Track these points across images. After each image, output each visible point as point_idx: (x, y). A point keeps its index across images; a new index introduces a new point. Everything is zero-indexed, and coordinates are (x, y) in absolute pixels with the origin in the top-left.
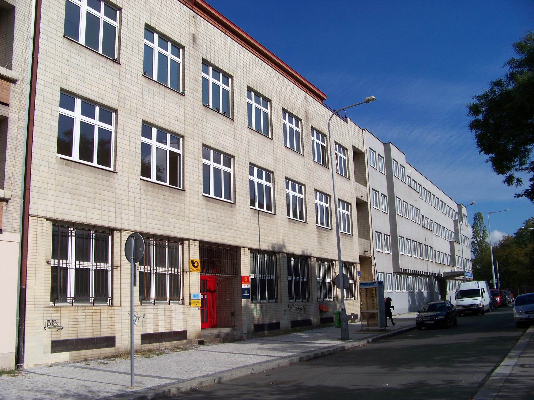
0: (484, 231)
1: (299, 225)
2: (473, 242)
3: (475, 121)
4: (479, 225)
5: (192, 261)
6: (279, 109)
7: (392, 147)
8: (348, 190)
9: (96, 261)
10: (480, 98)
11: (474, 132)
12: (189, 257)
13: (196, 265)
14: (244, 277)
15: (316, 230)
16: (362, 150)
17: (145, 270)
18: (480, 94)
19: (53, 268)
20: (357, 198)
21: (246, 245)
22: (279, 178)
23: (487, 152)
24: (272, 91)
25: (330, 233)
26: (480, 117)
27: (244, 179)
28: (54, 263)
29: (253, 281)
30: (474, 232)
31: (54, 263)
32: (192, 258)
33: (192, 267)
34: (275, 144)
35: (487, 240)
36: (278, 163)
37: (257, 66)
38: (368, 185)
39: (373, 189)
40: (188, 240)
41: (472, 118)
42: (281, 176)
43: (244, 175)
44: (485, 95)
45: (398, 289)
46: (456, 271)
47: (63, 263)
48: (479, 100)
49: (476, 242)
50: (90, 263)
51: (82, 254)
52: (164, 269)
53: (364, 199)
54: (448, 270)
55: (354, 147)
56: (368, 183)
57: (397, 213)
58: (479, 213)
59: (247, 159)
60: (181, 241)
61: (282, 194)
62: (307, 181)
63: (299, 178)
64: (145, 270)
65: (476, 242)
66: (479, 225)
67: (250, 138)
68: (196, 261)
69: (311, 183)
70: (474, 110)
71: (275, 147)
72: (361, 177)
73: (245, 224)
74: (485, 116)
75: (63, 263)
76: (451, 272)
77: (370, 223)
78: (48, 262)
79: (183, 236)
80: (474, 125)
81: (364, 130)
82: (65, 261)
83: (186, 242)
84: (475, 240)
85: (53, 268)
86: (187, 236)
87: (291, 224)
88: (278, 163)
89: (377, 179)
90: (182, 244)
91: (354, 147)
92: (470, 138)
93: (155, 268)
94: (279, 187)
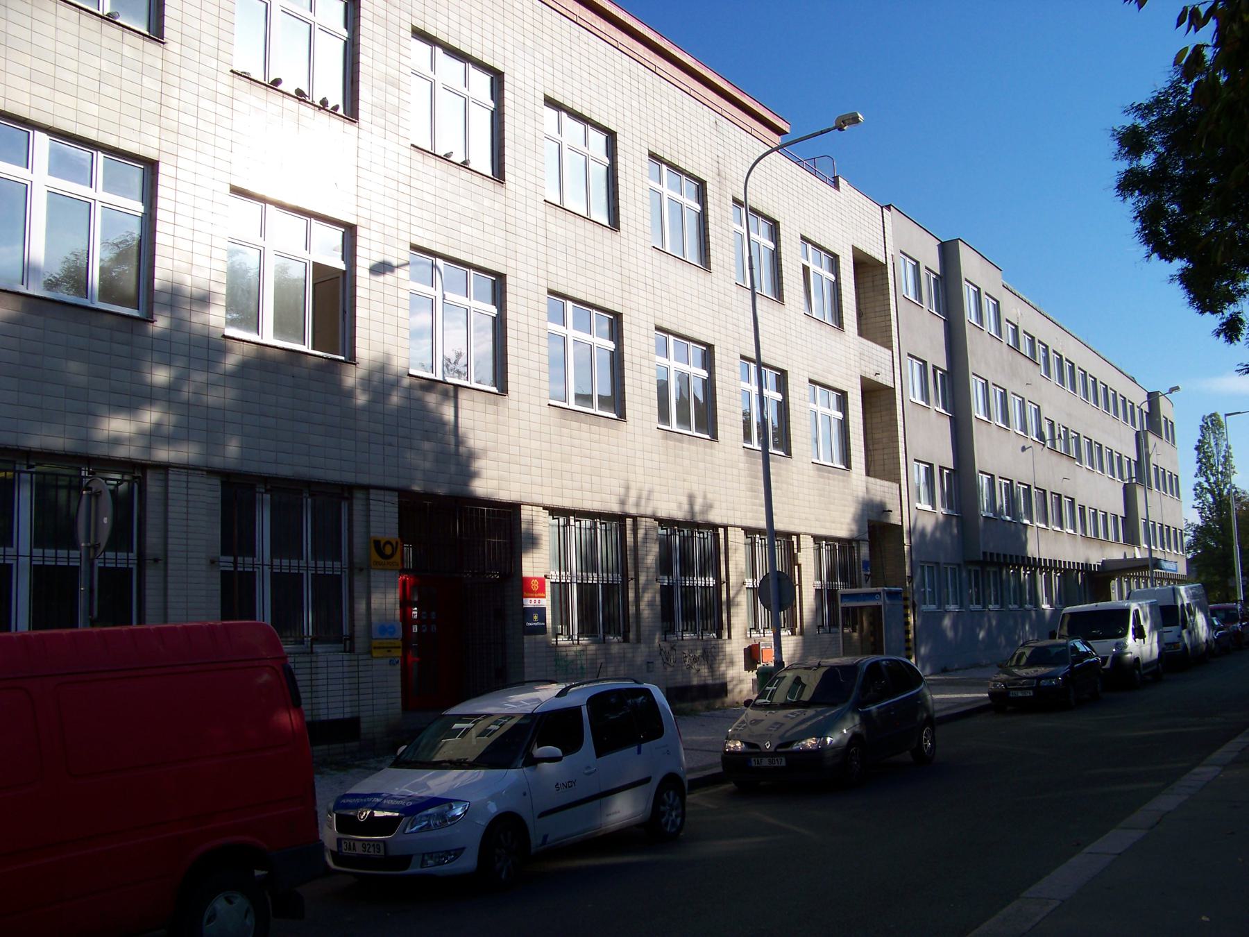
0: (1226, 458)
1: (693, 448)
2: (1199, 484)
3: (1130, 173)
4: (1213, 444)
5: (377, 543)
6: (638, 154)
7: (964, 251)
8: (849, 358)
9: (315, 558)
10: (1142, 110)
11: (1130, 200)
12: (369, 532)
13: (388, 550)
14: (529, 579)
15: (743, 458)
16: (882, 260)
17: (236, 567)
18: (1145, 97)
19: (224, 574)
20: (862, 378)
21: (537, 500)
22: (634, 328)
23: (1166, 253)
24: (620, 109)
25: (784, 466)
26: (1147, 161)
27: (534, 331)
28: (227, 563)
29: (561, 590)
30: (1199, 461)
31: (227, 563)
32: (377, 532)
33: (375, 557)
34: (624, 242)
35: (1235, 479)
36: (634, 290)
37: (574, 47)
38: (895, 344)
39: (909, 355)
40: (366, 488)
41: (1124, 165)
42: (643, 324)
43: (533, 322)
44: (1158, 102)
45: (978, 603)
46: (1138, 556)
47: (245, 563)
48: (1143, 117)
49: (1206, 485)
50: (303, 563)
51: (285, 542)
52: (337, 564)
53: (885, 379)
54: (1116, 553)
55: (856, 250)
56: (895, 339)
57: (975, 413)
58: (1214, 415)
59: (543, 282)
60: (346, 491)
61: (645, 370)
62: (717, 336)
63: (695, 328)
64: (236, 567)
65: (1206, 485)
66: (1213, 444)
67: (551, 227)
68: (388, 543)
69: (731, 340)
70: (1132, 142)
71: (625, 249)
72: (874, 326)
73: (535, 444)
74: (1160, 159)
75: (245, 563)
76: (1125, 560)
77: (901, 439)
78: (213, 562)
79: (349, 477)
80: (1129, 183)
81: (888, 207)
82: (249, 560)
83: (359, 495)
84: (1202, 480)
85: (224, 574)
86: (364, 479)
87: (671, 443)
88: (634, 290)
89: (919, 330)
90: (350, 499)
91: (856, 250)
92: (1124, 214)
93: (312, 564)
94: (636, 352)
